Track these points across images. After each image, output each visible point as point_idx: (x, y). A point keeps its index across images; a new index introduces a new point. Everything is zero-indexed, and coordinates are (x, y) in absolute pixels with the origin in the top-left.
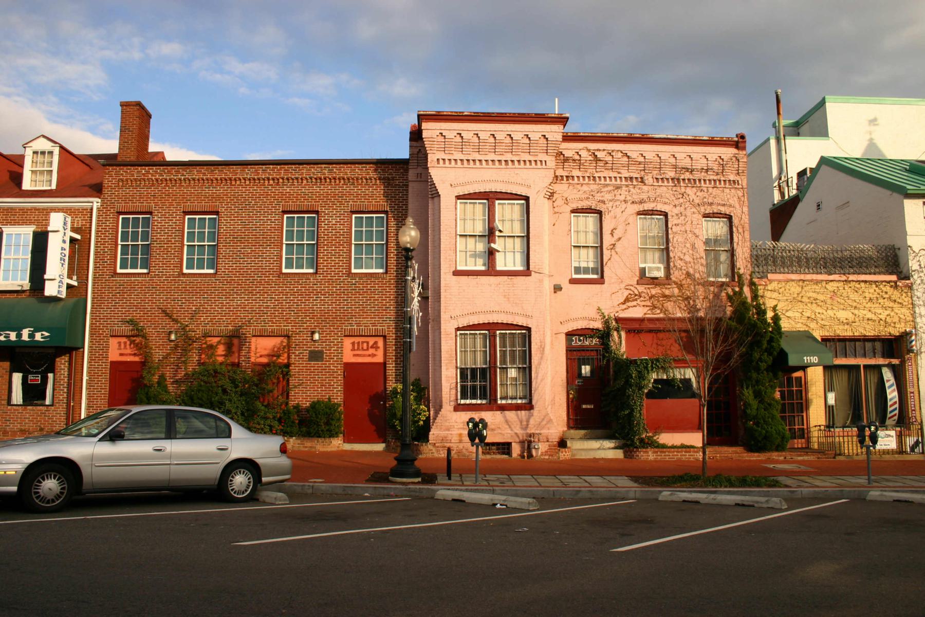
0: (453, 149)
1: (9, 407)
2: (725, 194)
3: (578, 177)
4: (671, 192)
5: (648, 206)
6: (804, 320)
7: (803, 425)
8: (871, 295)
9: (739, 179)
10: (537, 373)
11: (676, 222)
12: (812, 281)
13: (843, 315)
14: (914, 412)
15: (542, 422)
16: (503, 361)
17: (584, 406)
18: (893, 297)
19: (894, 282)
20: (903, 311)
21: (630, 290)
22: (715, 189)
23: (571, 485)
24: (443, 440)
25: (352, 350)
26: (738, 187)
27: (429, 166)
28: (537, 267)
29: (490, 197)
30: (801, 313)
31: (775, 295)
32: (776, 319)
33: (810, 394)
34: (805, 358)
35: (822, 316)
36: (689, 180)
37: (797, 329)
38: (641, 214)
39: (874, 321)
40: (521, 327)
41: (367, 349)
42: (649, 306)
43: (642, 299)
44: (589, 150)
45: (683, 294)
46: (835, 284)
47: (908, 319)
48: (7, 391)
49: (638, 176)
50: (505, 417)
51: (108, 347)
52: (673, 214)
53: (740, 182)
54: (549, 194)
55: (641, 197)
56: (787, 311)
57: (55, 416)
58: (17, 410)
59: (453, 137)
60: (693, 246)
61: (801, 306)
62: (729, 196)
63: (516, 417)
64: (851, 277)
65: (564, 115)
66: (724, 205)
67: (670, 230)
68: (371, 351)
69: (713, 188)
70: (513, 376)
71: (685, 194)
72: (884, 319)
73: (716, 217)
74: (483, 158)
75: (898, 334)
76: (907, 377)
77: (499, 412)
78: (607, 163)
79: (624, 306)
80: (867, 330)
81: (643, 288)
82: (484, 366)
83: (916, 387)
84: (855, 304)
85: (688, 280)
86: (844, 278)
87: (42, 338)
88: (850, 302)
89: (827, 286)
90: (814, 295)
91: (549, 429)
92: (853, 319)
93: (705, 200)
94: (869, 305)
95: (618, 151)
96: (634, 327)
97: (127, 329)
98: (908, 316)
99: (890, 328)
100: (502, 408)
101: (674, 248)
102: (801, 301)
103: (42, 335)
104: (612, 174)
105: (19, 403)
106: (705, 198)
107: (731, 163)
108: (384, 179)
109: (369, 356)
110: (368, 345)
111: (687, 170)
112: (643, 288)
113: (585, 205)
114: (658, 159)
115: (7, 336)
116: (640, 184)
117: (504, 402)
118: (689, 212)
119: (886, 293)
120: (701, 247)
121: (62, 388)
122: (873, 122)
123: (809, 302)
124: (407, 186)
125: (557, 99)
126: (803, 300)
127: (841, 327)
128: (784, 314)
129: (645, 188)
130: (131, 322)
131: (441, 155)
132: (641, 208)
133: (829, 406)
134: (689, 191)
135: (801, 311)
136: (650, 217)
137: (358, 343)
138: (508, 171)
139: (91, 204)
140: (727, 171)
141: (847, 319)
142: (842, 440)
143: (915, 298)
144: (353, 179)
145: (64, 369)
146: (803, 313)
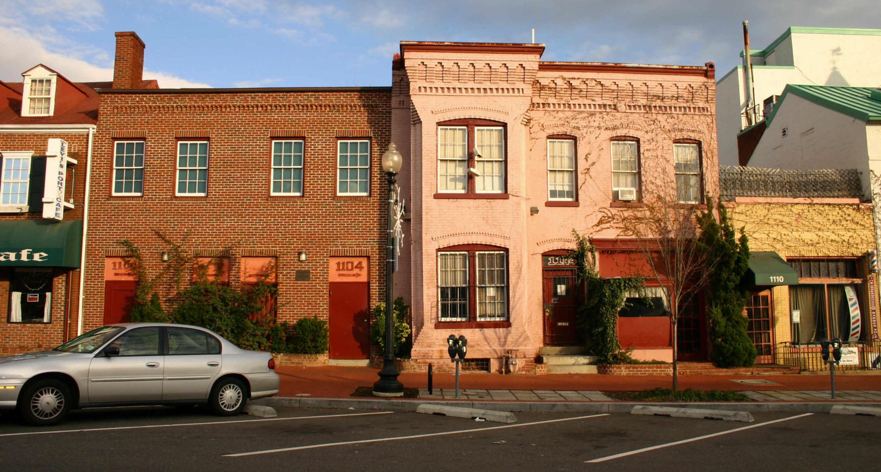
0: (434, 77)
1: (9, 325)
2: (695, 121)
3: (554, 104)
4: (643, 119)
5: (621, 132)
6: (770, 241)
7: (769, 342)
8: (834, 218)
9: (708, 107)
10: (514, 292)
11: (647, 147)
12: (777, 204)
13: (808, 236)
14: (875, 329)
15: (519, 338)
16: (482, 280)
17: (560, 324)
18: (856, 220)
19: (856, 204)
20: (865, 233)
21: (604, 212)
22: (685, 116)
23: (547, 399)
24: (425, 356)
25: (337, 270)
26: (707, 114)
27: (411, 94)
28: (515, 190)
29: (469, 124)
30: (768, 235)
31: (742, 217)
32: (744, 240)
33: (776, 312)
34: (771, 278)
35: (788, 238)
36: (660, 107)
37: (764, 250)
38: (614, 140)
39: (837, 242)
40: (499, 248)
41: (352, 269)
42: (621, 228)
43: (615, 221)
44: (564, 79)
45: (654, 216)
46: (800, 207)
47: (870, 240)
49: (611, 103)
50: (484, 334)
51: (103, 267)
52: (645, 140)
53: (709, 109)
54: (526, 121)
55: (614, 123)
56: (754, 232)
58: (16, 327)
59: (434, 66)
60: (664, 171)
61: (767, 227)
62: (698, 123)
63: (494, 334)
64: (816, 200)
65: (540, 45)
66: (693, 131)
67: (641, 155)
68: (356, 271)
69: (683, 114)
70: (492, 295)
71: (656, 121)
72: (846, 240)
73: (686, 143)
74: (462, 86)
75: (860, 255)
76: (869, 296)
77: (478, 330)
78: (581, 91)
79: (598, 228)
80: (831, 250)
81: (616, 211)
82: (464, 286)
83: (770, 305)
84: (819, 226)
85: (659, 203)
86: (808, 201)
87: (40, 258)
88: (814, 224)
89: (792, 208)
90: (780, 217)
91: (526, 346)
92: (817, 241)
93: (676, 126)
94: (833, 227)
95: (592, 79)
96: (607, 248)
97: (121, 250)
98: (870, 238)
99: (853, 249)
100: (481, 326)
101: (646, 172)
102: (767, 223)
103: (40, 255)
104: (587, 102)
105: (18, 321)
106: (675, 124)
107: (700, 91)
108: (368, 106)
109: (354, 275)
110: (352, 266)
111: (658, 97)
112: (616, 211)
113: (560, 131)
114: (631, 87)
115: (7, 257)
116: (613, 111)
117: (483, 319)
118: (660, 138)
119: (849, 215)
120: (672, 172)
121: (59, 307)
122: (836, 51)
123: (775, 224)
124: (390, 113)
125: (533, 30)
126: (769, 222)
127: (806, 248)
128: (751, 236)
129: (618, 115)
130: (126, 243)
131: (423, 84)
132: (614, 134)
133: (794, 324)
134: (660, 117)
135: (767, 232)
136: (622, 142)
137: (343, 263)
138: (486, 99)
139: (87, 130)
140: (697, 98)
141: (811, 240)
142: (807, 357)
143: (876, 221)
144: (338, 106)
146: (770, 235)
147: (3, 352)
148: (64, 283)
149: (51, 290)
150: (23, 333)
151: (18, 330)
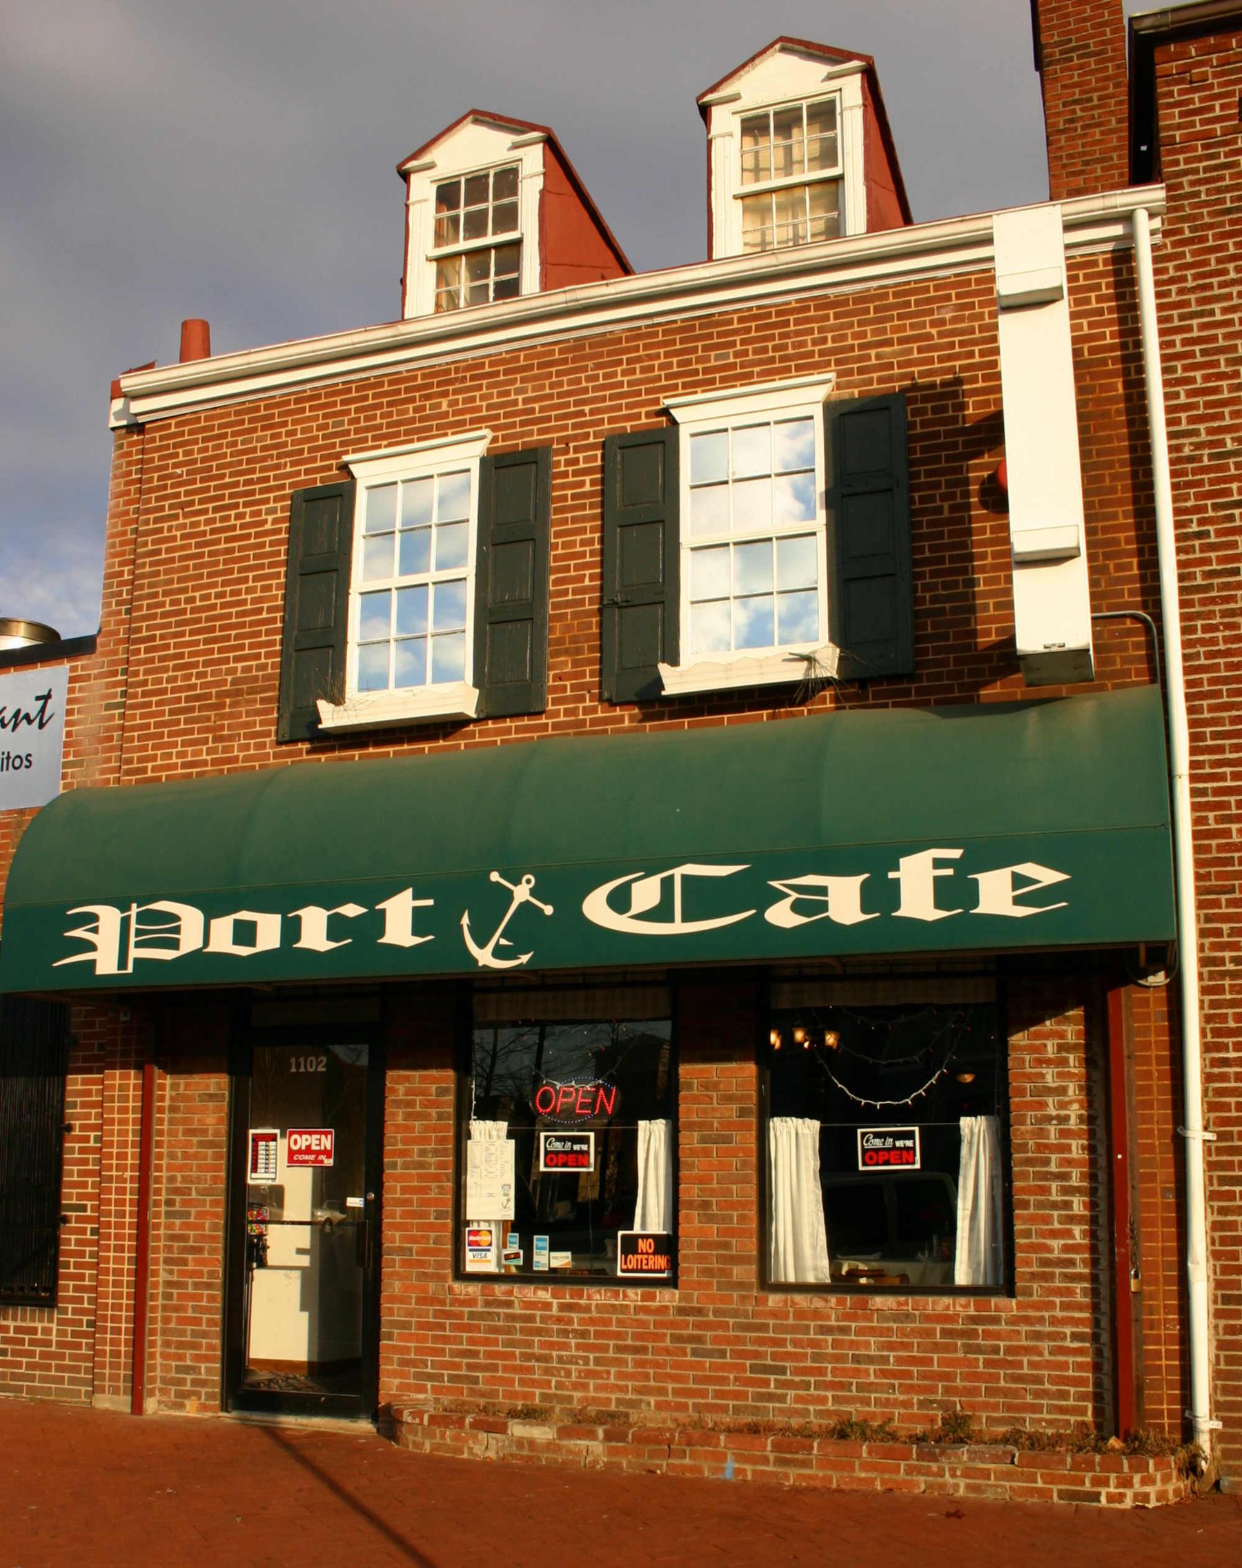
1: (774, 1300)
48: (753, 1213)
57: (1027, 1350)
58: (816, 1314)
87: (1018, 901)
103: (1019, 881)
105: (811, 1279)
115: (812, 903)
121: (1055, 1197)
139: (1117, 230)
145: (1063, 1091)
147: (780, 1462)
148: (1074, 1062)
149: (666, 1107)
150: (853, 1345)
151: (829, 1330)
